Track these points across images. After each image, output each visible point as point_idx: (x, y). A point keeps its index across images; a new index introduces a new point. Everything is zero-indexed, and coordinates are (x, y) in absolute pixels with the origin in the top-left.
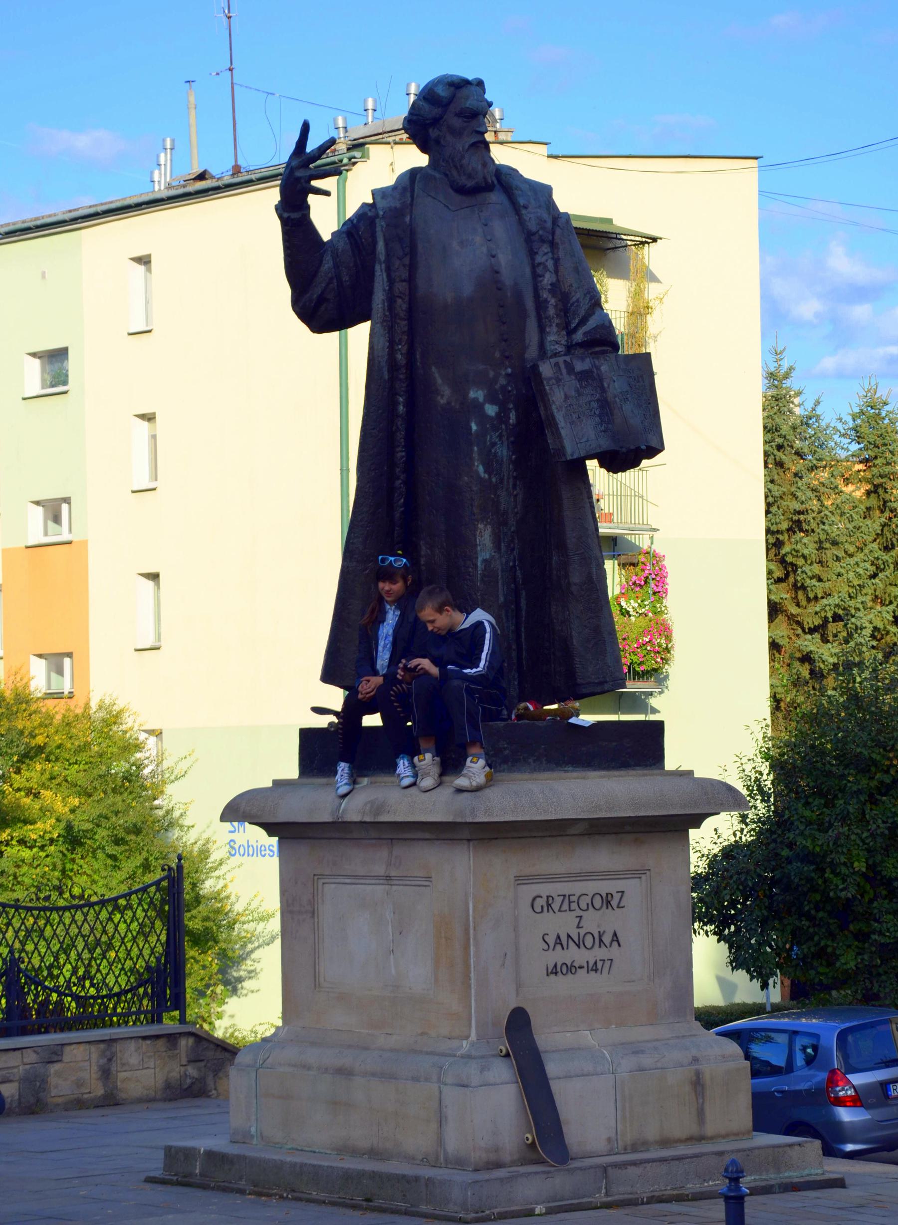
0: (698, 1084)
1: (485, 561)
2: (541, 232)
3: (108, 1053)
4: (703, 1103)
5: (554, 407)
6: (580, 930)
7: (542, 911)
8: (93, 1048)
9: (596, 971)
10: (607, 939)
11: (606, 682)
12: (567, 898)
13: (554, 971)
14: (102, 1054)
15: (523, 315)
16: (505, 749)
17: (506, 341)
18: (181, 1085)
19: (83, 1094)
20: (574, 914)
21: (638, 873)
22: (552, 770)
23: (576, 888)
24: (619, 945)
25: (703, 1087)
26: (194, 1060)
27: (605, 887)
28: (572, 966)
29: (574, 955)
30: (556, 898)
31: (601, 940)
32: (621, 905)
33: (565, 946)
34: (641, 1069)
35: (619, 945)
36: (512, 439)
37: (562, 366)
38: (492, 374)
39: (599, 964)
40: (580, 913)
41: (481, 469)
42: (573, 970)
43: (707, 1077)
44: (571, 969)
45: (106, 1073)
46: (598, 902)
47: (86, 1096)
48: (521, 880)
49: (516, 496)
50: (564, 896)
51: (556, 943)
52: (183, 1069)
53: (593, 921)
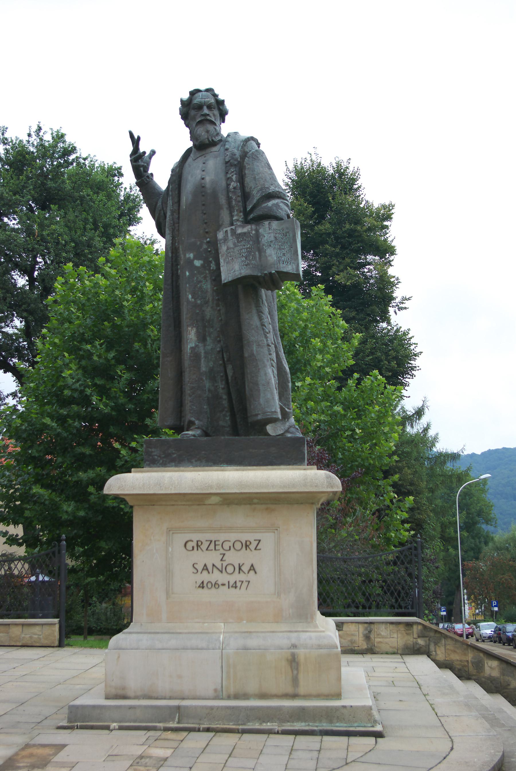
0: (293, 662)
1: (192, 348)
2: (231, 161)
3: (369, 629)
4: (297, 674)
5: (220, 255)
6: (223, 562)
7: (193, 549)
8: (361, 626)
9: (236, 587)
10: (245, 568)
11: (259, 414)
12: (213, 543)
13: (202, 586)
14: (366, 629)
15: (219, 208)
16: (174, 454)
17: (206, 223)
18: (413, 647)
19: (354, 647)
20: (218, 553)
21: (274, 529)
22: (211, 466)
23: (221, 537)
24: (256, 573)
25: (298, 664)
26: (421, 636)
27: (244, 537)
28: (215, 583)
29: (216, 576)
30: (204, 542)
31: (240, 569)
32: (258, 548)
33: (211, 572)
34: (246, 648)
35: (256, 573)
36: (213, 278)
37: (229, 232)
38: (198, 243)
39: (238, 584)
40: (224, 552)
41: (190, 296)
42: (217, 586)
43: (302, 659)
44: (216, 585)
45: (367, 638)
46: (238, 546)
47: (356, 648)
48: (171, 531)
49: (219, 310)
50: (211, 541)
51: (203, 569)
52: (415, 640)
53: (234, 558)
